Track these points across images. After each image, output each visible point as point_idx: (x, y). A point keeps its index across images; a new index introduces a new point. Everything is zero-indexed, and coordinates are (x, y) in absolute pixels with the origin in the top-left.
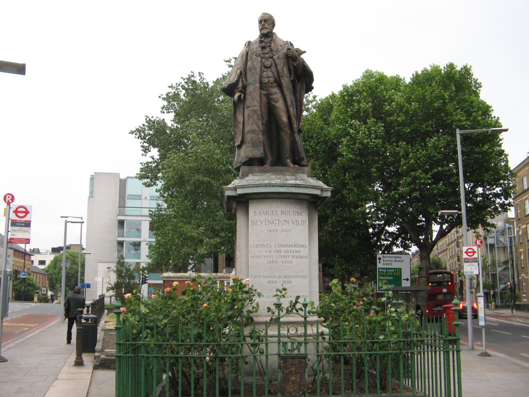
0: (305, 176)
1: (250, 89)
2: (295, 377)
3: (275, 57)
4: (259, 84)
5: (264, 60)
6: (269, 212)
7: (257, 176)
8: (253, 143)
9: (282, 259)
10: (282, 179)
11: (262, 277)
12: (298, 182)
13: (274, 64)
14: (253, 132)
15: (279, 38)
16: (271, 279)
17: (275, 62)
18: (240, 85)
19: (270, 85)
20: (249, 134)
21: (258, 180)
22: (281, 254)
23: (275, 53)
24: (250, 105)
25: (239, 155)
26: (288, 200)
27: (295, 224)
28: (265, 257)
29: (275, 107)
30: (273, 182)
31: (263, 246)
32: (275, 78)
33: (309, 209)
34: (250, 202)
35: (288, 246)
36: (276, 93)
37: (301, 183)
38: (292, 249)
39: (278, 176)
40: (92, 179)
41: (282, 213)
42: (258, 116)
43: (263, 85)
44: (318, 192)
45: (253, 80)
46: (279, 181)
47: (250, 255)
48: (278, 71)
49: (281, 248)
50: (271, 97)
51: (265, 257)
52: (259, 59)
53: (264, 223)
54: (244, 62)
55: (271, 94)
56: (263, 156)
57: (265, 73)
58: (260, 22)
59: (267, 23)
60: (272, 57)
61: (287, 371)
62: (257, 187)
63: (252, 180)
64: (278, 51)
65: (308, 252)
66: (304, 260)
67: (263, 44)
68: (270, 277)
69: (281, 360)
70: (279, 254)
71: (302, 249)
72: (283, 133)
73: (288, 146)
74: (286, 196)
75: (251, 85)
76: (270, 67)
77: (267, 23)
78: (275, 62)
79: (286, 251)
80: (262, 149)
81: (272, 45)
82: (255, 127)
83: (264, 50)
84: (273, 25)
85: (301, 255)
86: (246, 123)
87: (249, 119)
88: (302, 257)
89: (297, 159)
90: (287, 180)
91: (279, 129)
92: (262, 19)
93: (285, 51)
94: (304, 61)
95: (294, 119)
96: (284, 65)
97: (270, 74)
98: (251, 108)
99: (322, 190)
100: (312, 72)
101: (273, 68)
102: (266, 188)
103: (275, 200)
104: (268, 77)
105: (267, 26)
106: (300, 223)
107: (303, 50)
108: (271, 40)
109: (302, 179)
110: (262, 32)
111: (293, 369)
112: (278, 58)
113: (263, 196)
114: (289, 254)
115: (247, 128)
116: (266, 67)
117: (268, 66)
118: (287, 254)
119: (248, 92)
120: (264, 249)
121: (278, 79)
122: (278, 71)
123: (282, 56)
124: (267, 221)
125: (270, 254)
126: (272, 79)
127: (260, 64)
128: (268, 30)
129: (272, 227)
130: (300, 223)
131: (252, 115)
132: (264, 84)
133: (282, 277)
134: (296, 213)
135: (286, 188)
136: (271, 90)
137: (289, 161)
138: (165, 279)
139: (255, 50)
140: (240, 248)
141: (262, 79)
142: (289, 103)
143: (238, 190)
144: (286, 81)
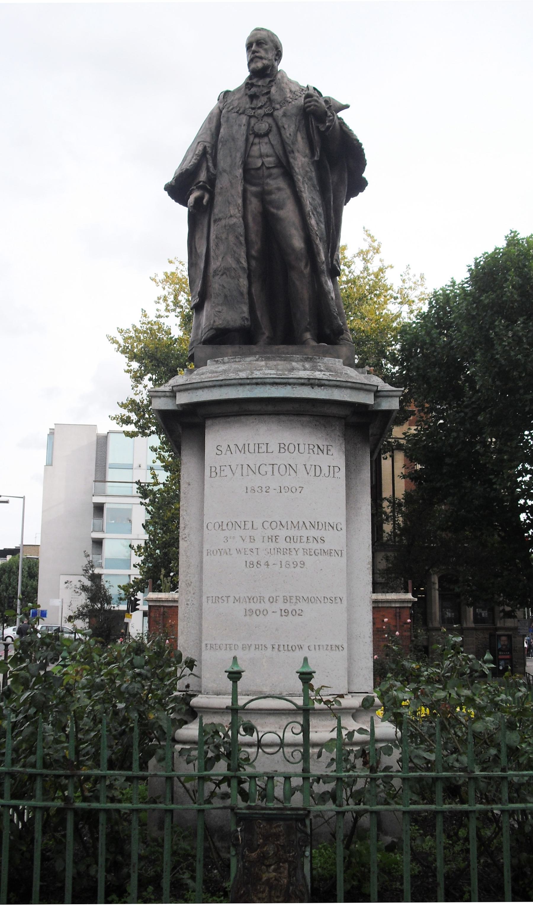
0: (338, 363)
1: (223, 182)
2: (275, 870)
3: (278, 113)
4: (241, 171)
5: (253, 121)
6: (252, 446)
7: (224, 363)
8: (226, 296)
9: (281, 557)
10: (280, 367)
11: (231, 599)
12: (318, 375)
13: (274, 129)
14: (226, 271)
15: (289, 80)
16: (254, 606)
17: (277, 124)
18: (203, 176)
19: (266, 172)
20: (217, 278)
21: (225, 371)
22: (278, 546)
23: (278, 106)
24: (220, 216)
26: (296, 418)
27: (312, 473)
28: (239, 551)
29: (277, 219)
30: (257, 374)
31: (235, 525)
32: (278, 158)
33: (347, 440)
35: (295, 526)
36: (279, 189)
37: (325, 377)
38: (304, 533)
39: (272, 363)
40: (52, 433)
41: (282, 447)
42: (237, 238)
43: (249, 174)
44: (368, 399)
45: (229, 163)
47: (206, 547)
48: (283, 143)
49: (277, 532)
50: (268, 198)
51: (239, 551)
52: (244, 119)
55: (270, 193)
57: (255, 148)
58: (249, 46)
59: (263, 50)
60: (271, 115)
61: (254, 855)
62: (221, 386)
63: (213, 372)
64: (285, 101)
65: (344, 540)
66: (335, 559)
67: (254, 90)
68: (251, 599)
70: (273, 545)
71: (328, 534)
72: (294, 276)
73: (307, 302)
75: (225, 174)
76: (266, 134)
77: (263, 50)
78: (277, 124)
79: (289, 539)
80: (245, 309)
81: (273, 90)
82: (231, 262)
83: (255, 102)
84: (279, 55)
85: (326, 547)
86: (212, 254)
87: (217, 245)
88: (328, 553)
89: (328, 331)
90: (293, 369)
91: (287, 267)
92: (253, 39)
93: (301, 101)
94: (344, 123)
95: (318, 241)
96: (298, 130)
97: (265, 149)
98: (223, 222)
99: (378, 394)
100: (361, 145)
101: (273, 137)
102: (240, 389)
103: (266, 418)
104: (261, 156)
105: (262, 53)
106: (325, 470)
107: (344, 103)
108: (271, 81)
109: (328, 369)
110: (253, 66)
111: (270, 849)
112: (285, 115)
113: (236, 408)
114: (298, 546)
115: (214, 265)
116: (258, 135)
117: (262, 132)
118: (292, 545)
119: (217, 190)
120: (239, 532)
121: (283, 160)
122: (283, 143)
123: (294, 111)
124: (245, 467)
126: (271, 159)
127: (244, 128)
128: (265, 62)
129: (257, 481)
130: (325, 470)
131: (224, 236)
132: (253, 172)
133: (280, 599)
134: (316, 449)
135: (289, 387)
136: (267, 184)
137: (308, 335)
138: (151, 604)
139: (236, 103)
140: (186, 531)
141: (250, 160)
142: (308, 208)
143: (178, 394)
144: (301, 162)
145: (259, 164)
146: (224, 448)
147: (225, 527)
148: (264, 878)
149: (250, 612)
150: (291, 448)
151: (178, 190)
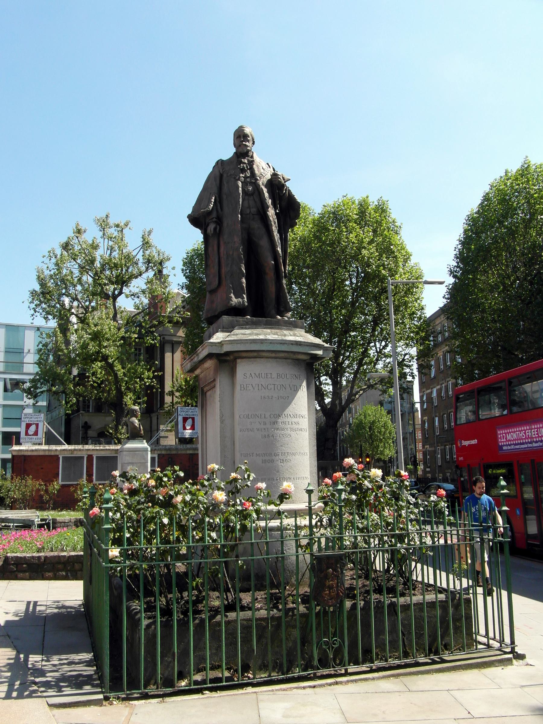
0: (302, 332)
6: (263, 375)
11: (255, 455)
16: (267, 458)
25: (212, 302)
28: (258, 430)
34: (238, 361)
46: (276, 336)
53: (256, 388)
54: (218, 185)
56: (235, 619)
69: (315, 559)
74: (282, 355)
124: (260, 386)
125: (264, 427)
145: (248, 212)
146: (248, 376)
147: (250, 417)
148: (327, 585)
149: (264, 461)
150: (283, 376)
151: (196, 220)
